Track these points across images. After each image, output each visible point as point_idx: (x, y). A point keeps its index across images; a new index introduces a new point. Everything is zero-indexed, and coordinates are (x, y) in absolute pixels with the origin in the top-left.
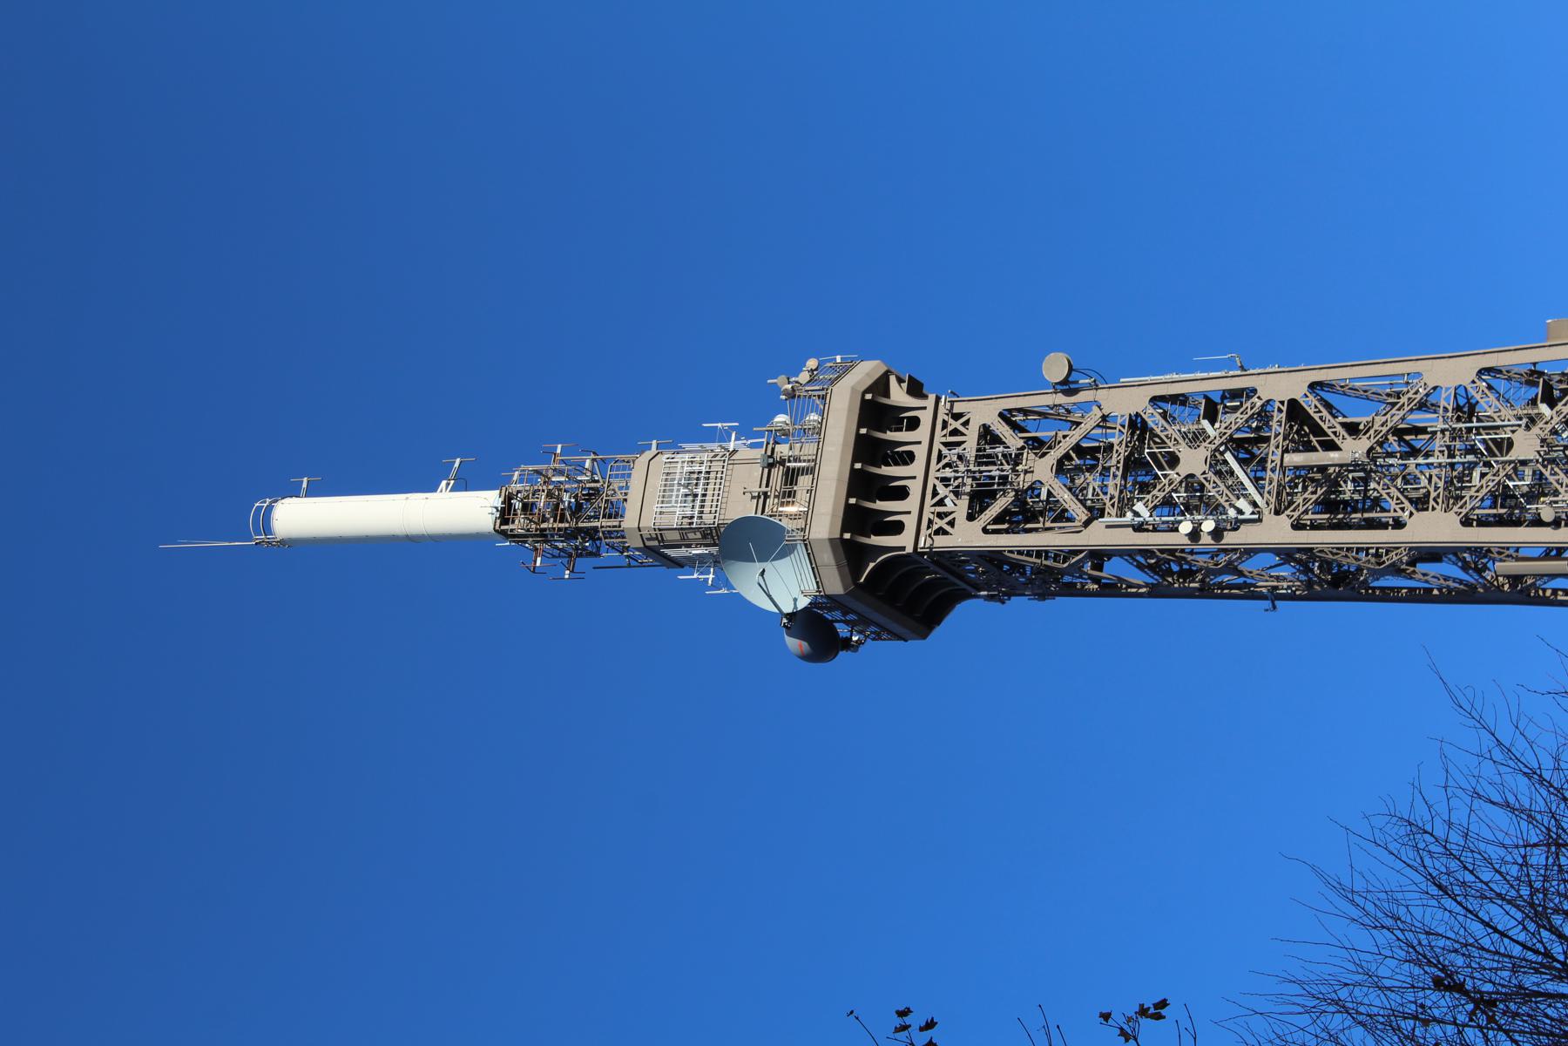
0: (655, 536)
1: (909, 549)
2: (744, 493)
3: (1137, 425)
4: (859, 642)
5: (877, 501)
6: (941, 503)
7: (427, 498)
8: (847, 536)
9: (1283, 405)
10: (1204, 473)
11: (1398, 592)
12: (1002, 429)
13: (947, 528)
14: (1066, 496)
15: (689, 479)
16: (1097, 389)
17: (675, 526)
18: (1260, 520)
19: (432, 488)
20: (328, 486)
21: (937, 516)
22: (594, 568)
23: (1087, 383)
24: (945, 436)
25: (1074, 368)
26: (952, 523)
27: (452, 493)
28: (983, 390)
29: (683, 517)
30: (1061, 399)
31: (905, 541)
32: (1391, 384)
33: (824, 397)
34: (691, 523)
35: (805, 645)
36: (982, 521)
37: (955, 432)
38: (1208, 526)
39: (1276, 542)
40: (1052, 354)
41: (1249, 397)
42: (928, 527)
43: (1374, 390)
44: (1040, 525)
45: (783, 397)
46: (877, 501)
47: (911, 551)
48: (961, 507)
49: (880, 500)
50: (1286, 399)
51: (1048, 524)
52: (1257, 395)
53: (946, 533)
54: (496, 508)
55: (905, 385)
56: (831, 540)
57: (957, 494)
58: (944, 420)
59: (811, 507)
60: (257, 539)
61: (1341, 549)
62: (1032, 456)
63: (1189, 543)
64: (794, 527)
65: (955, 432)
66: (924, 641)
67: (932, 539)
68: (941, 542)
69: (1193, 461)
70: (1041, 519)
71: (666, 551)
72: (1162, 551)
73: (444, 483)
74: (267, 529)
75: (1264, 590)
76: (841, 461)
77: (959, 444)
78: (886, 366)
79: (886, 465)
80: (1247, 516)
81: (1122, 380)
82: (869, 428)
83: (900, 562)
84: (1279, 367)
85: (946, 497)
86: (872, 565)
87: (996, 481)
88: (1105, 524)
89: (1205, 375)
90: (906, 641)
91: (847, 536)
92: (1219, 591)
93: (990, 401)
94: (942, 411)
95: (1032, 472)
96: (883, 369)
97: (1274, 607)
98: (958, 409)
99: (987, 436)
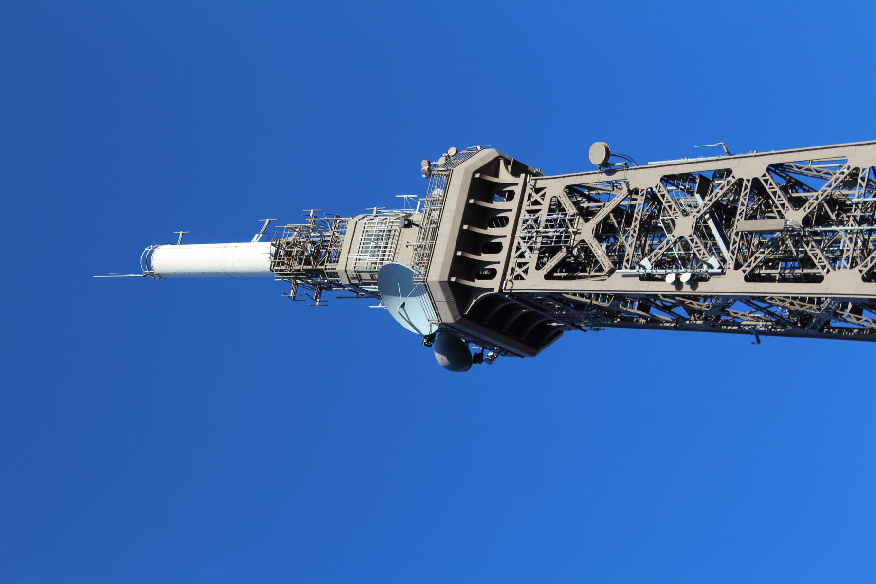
0: (355, 276)
1: (496, 291)
2: (407, 246)
3: (652, 197)
4: (493, 358)
5: (482, 254)
6: (522, 256)
7: (236, 247)
8: (453, 279)
9: (749, 183)
10: (690, 236)
11: (852, 332)
12: (566, 202)
13: (523, 275)
14: (599, 252)
15: (378, 235)
16: (627, 170)
17: (365, 270)
18: (723, 273)
19: (248, 239)
20: (192, 238)
21: (518, 266)
22: (338, 298)
23: (620, 166)
24: (529, 205)
25: (611, 153)
26: (526, 271)
27: (259, 243)
28: (557, 171)
29: (372, 263)
30: (604, 177)
31: (494, 284)
32: (841, 166)
33: (448, 176)
34: (375, 268)
35: (445, 358)
36: (545, 270)
37: (536, 203)
38: (685, 277)
39: (733, 291)
40: (596, 143)
41: (728, 175)
42: (511, 274)
43: (826, 171)
44: (587, 274)
45: (424, 176)
46: (482, 254)
47: (497, 292)
48: (531, 258)
49: (485, 253)
50: (751, 178)
51: (593, 273)
52: (732, 175)
53: (522, 279)
54: (271, 254)
55: (510, 167)
56: (441, 283)
57: (531, 249)
58: (529, 193)
59: (430, 258)
60: (145, 273)
61: (788, 298)
62: (581, 221)
63: (692, 291)
64: (549, 263)
65: (536, 203)
66: (528, 359)
67: (512, 282)
68: (519, 285)
69: (684, 227)
70: (588, 269)
71: (364, 287)
72: (664, 296)
73: (257, 235)
74: (150, 268)
75: (747, 328)
76: (453, 223)
77: (537, 211)
78: (498, 152)
79: (490, 227)
80: (716, 270)
81: (649, 163)
82: (476, 198)
83: (493, 300)
84: (757, 152)
85: (525, 251)
86: (474, 301)
87: (554, 240)
88: (622, 274)
89: (704, 159)
90: (523, 357)
91: (453, 279)
92: (725, 327)
93: (560, 179)
94: (528, 187)
95: (580, 233)
96: (497, 154)
97: (758, 341)
98: (539, 185)
99: (556, 206)
